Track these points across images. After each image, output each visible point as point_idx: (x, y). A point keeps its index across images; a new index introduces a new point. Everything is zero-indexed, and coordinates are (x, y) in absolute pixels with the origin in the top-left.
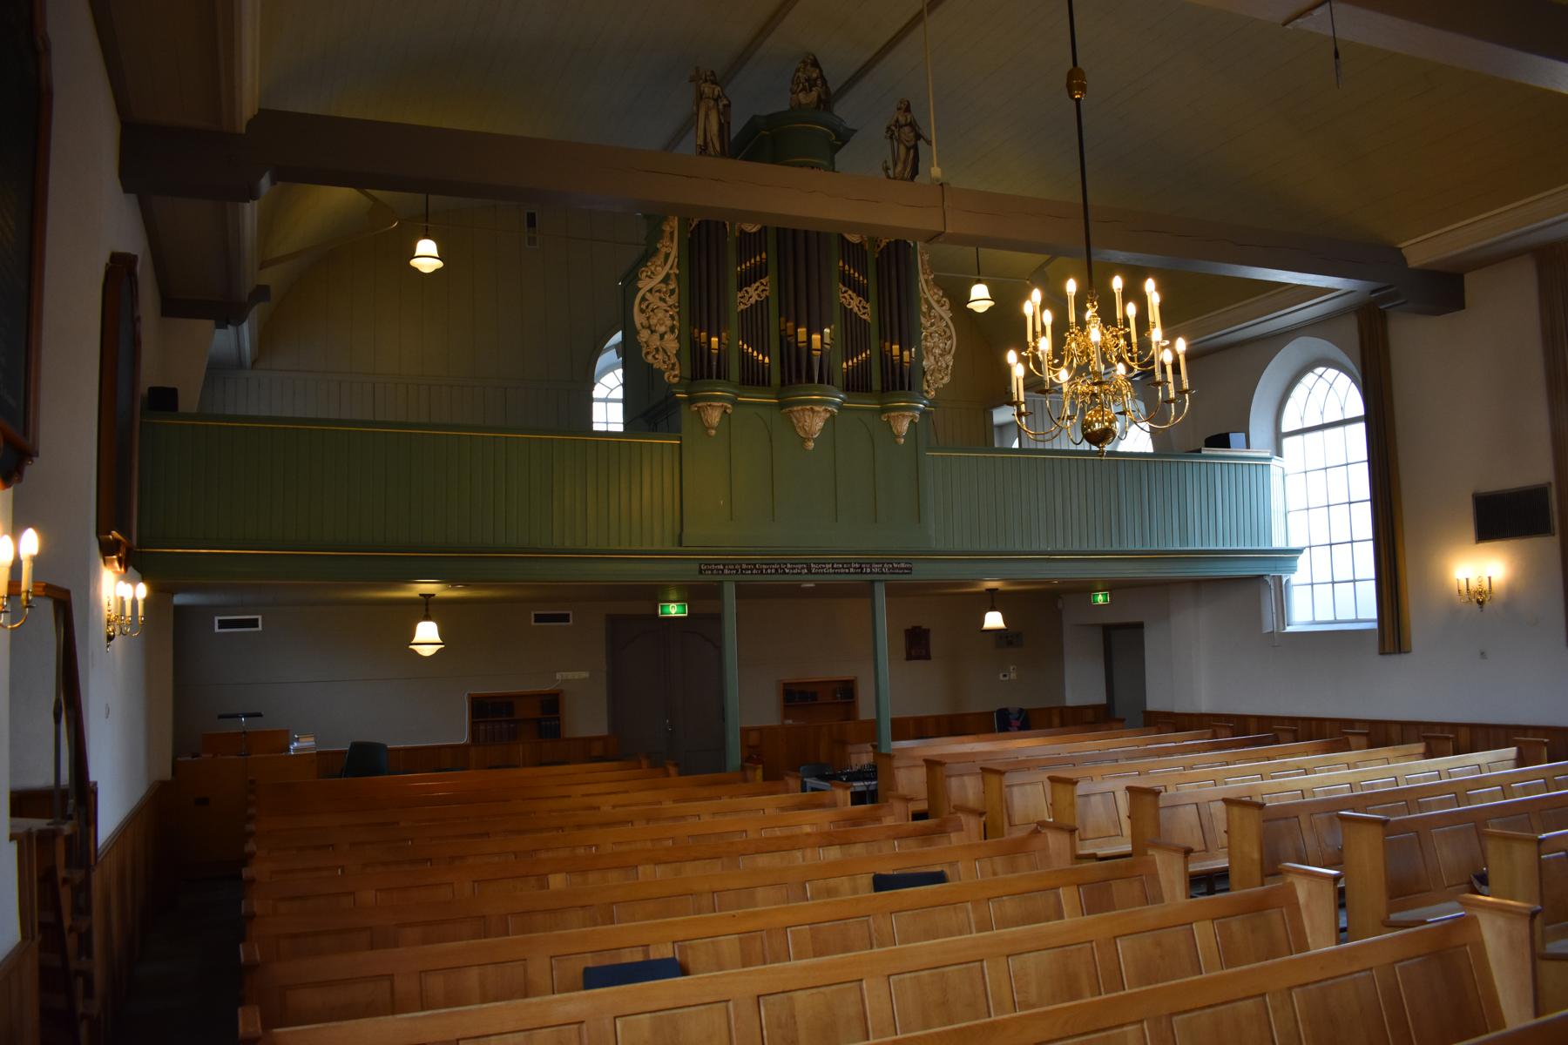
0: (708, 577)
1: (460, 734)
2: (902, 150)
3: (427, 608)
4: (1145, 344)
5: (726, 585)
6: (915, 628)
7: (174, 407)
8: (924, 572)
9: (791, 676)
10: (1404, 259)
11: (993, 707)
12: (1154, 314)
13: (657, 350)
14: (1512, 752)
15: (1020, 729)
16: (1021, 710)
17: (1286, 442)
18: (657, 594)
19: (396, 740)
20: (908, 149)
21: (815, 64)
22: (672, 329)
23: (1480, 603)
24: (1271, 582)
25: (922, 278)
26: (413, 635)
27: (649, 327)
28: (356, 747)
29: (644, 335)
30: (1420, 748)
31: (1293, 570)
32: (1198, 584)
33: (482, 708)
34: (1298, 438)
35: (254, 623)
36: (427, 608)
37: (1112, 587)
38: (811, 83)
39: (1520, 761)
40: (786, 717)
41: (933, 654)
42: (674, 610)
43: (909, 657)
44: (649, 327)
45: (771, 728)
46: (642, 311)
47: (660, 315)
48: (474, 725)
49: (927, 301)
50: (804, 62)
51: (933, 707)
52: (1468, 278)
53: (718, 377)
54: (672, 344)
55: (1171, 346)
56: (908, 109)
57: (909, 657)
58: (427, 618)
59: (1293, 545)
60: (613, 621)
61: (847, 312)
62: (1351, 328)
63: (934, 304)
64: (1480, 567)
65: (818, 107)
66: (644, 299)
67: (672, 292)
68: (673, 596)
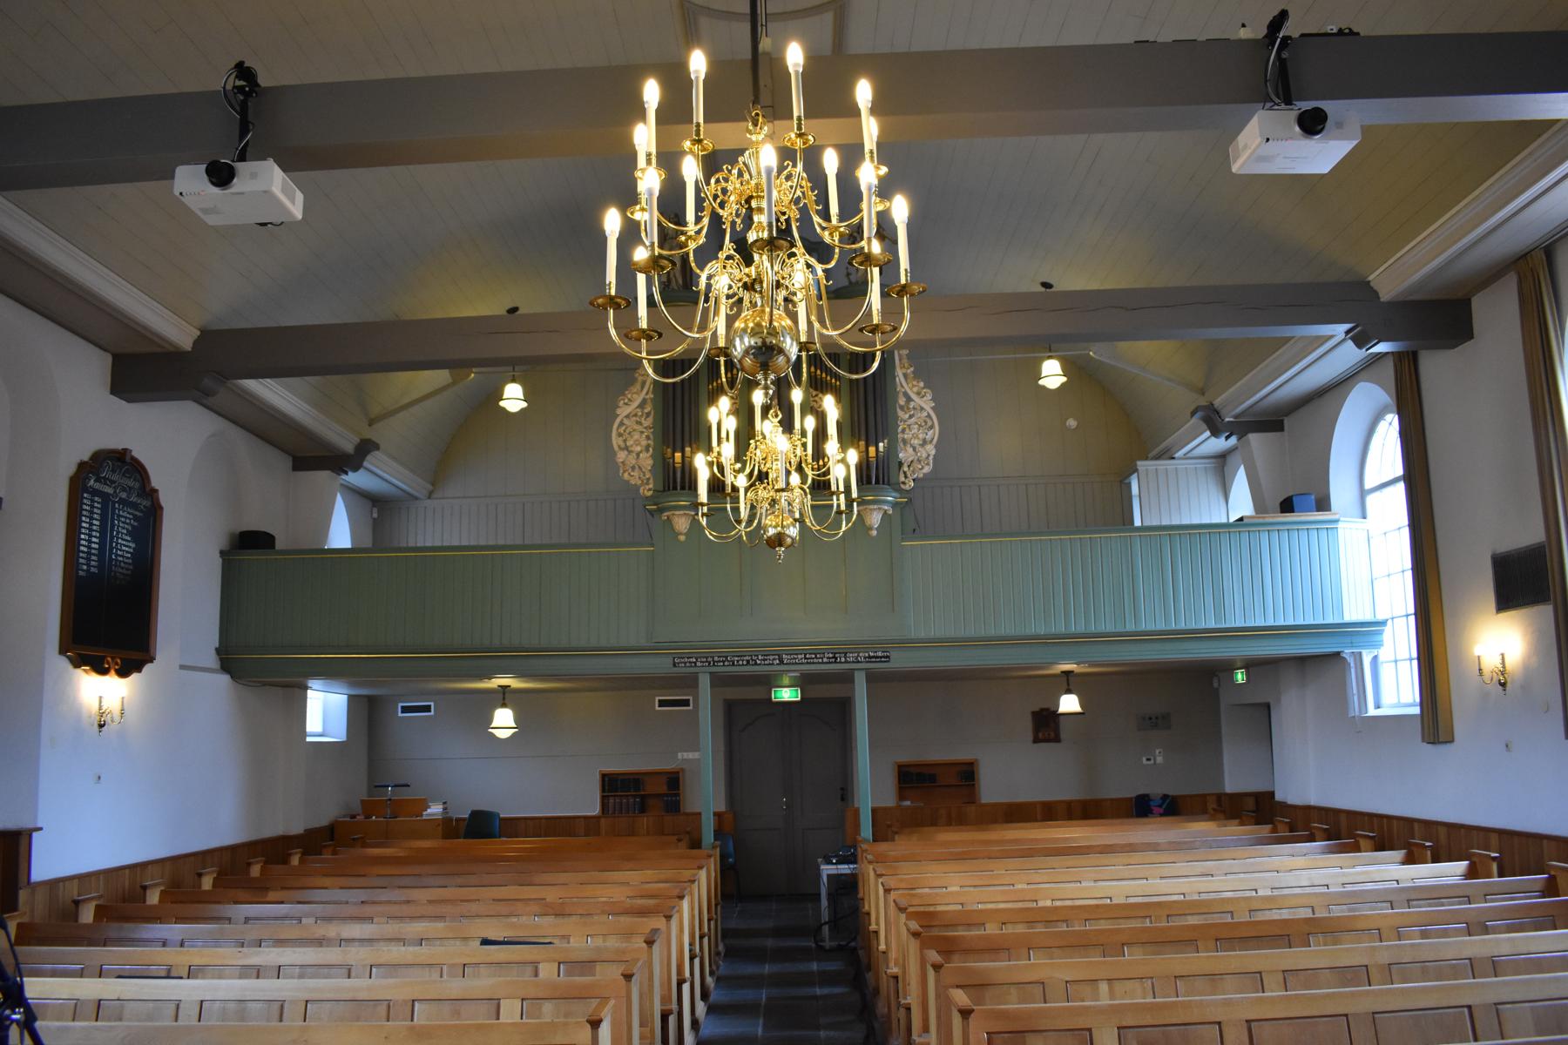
0: (681, 670)
1: (589, 804)
3: (504, 697)
4: (819, 454)
5: (701, 676)
6: (1042, 710)
7: (273, 546)
8: (901, 661)
9: (905, 758)
10: (1376, 293)
11: (1131, 793)
12: (832, 429)
13: (633, 468)
14: (1461, 866)
15: (1161, 815)
16: (1165, 797)
17: (1370, 499)
18: (769, 682)
22: (648, 447)
23: (1503, 685)
24: (1351, 660)
25: (899, 372)
27: (627, 448)
29: (621, 456)
30: (1399, 854)
31: (1378, 645)
32: (1302, 661)
33: (611, 784)
34: (1377, 494)
35: (428, 709)
36: (504, 697)
37: (1250, 665)
39: (1472, 873)
40: (901, 797)
41: (1063, 735)
42: (787, 694)
43: (1036, 740)
44: (627, 448)
45: (885, 809)
46: (620, 435)
47: (636, 436)
49: (906, 394)
52: (1476, 303)
53: (683, 488)
54: (647, 461)
55: (843, 461)
57: (1036, 740)
58: (504, 705)
59: (1380, 617)
62: (1388, 369)
63: (913, 396)
64: (1501, 642)
66: (622, 424)
67: (648, 415)
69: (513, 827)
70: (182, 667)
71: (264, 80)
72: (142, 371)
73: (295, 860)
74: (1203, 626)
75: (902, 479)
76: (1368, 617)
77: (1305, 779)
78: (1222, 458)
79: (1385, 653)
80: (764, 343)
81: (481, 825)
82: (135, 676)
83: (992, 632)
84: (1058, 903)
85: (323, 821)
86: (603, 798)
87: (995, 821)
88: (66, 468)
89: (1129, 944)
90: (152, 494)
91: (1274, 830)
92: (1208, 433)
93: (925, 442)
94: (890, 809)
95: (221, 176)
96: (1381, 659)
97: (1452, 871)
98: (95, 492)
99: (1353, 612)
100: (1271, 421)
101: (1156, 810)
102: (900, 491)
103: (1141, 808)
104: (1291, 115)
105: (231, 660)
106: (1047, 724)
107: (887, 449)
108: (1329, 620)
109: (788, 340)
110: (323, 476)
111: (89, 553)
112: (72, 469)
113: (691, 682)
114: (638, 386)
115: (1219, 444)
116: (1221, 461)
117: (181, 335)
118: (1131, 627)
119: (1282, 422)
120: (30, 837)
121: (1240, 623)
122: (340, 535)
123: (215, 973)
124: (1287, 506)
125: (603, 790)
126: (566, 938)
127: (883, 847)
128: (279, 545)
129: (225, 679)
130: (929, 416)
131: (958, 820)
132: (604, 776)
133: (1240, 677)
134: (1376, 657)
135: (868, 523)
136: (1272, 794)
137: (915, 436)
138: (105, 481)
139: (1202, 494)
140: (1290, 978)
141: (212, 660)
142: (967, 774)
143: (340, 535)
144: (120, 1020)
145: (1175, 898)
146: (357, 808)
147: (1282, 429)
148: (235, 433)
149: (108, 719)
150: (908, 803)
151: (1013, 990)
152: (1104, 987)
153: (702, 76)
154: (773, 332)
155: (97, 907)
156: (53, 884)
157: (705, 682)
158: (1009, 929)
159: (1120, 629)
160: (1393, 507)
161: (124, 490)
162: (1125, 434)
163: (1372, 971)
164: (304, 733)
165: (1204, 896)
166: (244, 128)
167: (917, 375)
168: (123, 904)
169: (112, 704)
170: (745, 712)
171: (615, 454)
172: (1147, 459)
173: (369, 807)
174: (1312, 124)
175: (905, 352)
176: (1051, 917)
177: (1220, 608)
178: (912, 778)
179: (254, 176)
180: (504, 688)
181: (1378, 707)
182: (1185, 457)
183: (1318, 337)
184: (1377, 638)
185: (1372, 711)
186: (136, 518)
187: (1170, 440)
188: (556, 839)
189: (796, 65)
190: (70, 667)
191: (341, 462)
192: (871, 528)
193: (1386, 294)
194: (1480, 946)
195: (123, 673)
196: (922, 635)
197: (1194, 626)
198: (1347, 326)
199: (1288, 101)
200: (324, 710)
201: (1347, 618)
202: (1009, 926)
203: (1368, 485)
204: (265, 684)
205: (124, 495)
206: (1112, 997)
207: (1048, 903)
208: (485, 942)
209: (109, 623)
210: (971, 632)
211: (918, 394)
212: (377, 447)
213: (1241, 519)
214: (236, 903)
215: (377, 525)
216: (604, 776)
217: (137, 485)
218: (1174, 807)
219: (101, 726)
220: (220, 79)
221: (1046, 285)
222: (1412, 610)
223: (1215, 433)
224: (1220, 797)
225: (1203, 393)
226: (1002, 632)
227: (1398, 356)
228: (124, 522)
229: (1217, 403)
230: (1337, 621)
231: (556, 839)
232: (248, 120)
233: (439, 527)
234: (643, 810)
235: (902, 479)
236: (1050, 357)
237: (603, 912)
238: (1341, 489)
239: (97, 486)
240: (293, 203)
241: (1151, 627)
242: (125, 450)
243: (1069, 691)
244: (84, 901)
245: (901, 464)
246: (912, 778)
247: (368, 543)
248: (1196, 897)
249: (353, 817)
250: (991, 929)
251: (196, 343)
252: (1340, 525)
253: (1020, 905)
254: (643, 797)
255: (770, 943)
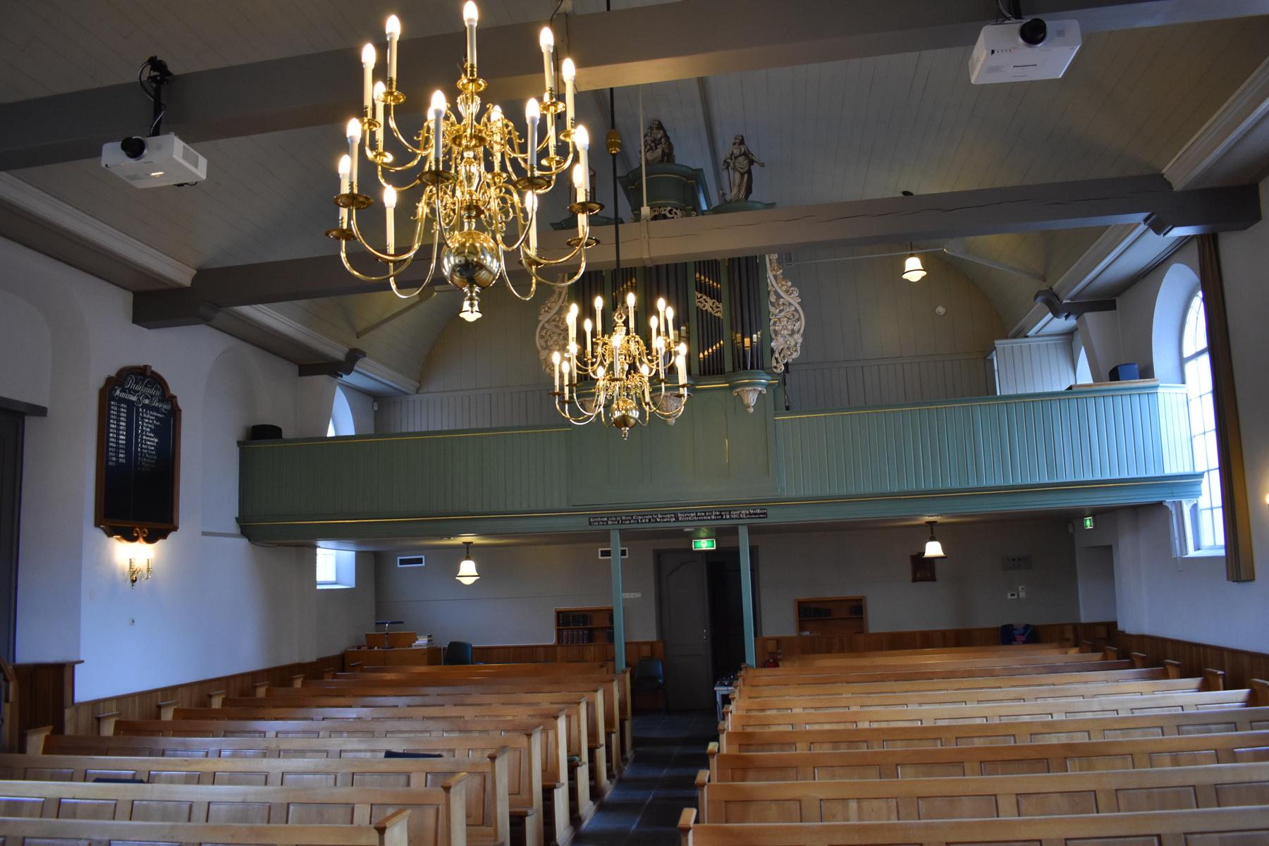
0: (596, 527)
2: (737, 176)
3: (468, 551)
8: (776, 517)
10: (1169, 185)
11: (999, 623)
14: (1243, 693)
15: (1025, 642)
16: (1027, 627)
17: (1189, 367)
19: (478, 641)
20: (742, 175)
21: (660, 126)
25: (770, 274)
26: (458, 571)
28: (453, 645)
30: (1195, 682)
32: (1136, 510)
33: (565, 619)
35: (420, 561)
37: (1097, 513)
38: (656, 142)
39: (1252, 701)
40: (801, 628)
42: (704, 545)
43: (915, 580)
46: (542, 337)
47: (555, 338)
48: (559, 632)
49: (776, 293)
50: (651, 128)
51: (941, 621)
56: (742, 142)
57: (915, 580)
58: (468, 558)
59: (1198, 470)
60: (659, 556)
61: (702, 313)
62: (1193, 251)
63: (782, 294)
65: (662, 161)
66: (543, 328)
68: (703, 535)
69: (486, 655)
70: (204, 534)
71: (175, 68)
72: (156, 304)
73: (298, 684)
74: (1037, 481)
75: (774, 364)
76: (1188, 470)
77: (1141, 614)
78: (1070, 334)
79: (1203, 502)
80: (467, 261)
81: (457, 654)
82: (160, 542)
83: (853, 491)
84: (875, 725)
85: (335, 650)
86: (558, 631)
87: (880, 649)
88: (96, 381)
89: (902, 765)
90: (172, 400)
91: (1105, 658)
92: (1050, 315)
93: (793, 333)
94: (792, 638)
95: (134, 149)
96: (1201, 506)
97: (1234, 698)
98: (121, 400)
99: (1174, 465)
100: (1106, 300)
101: (1018, 637)
102: (771, 374)
103: (1006, 636)
104: (1015, 26)
105: (249, 527)
106: (923, 568)
107: (761, 340)
108: (1152, 474)
109: (489, 258)
110: (322, 379)
111: (117, 448)
112: (101, 383)
113: (605, 537)
114: (556, 296)
115: (1062, 323)
116: (1069, 336)
117: (182, 275)
118: (973, 484)
119: (1114, 301)
120: (73, 668)
121: (1070, 479)
122: (342, 422)
123: (219, 775)
124: (1114, 375)
125: (558, 624)
126: (452, 751)
127: (766, 674)
128: (285, 435)
129: (244, 542)
130: (796, 310)
131: (850, 648)
132: (559, 613)
133: (1088, 523)
134: (1195, 506)
135: (746, 402)
136: (1115, 623)
137: (785, 328)
138: (131, 391)
139: (1045, 365)
140: (1024, 803)
141: (233, 527)
142: (857, 608)
143: (342, 422)
144: (75, 817)
145: (978, 721)
146: (364, 640)
147: (1114, 308)
148: (245, 348)
149: (138, 576)
150: (807, 633)
151: (774, 807)
152: (853, 805)
153: (396, 38)
154: (473, 250)
155: (117, 722)
156: (95, 704)
157: (615, 537)
158: (817, 750)
159: (964, 486)
160: (1201, 373)
161: (146, 397)
162: (982, 319)
163: (1101, 797)
164: (315, 583)
165: (1005, 720)
166: (158, 108)
167: (786, 277)
168: (144, 722)
169: (141, 564)
170: (666, 556)
171: (538, 352)
172: (1006, 338)
173: (372, 640)
174: (1034, 34)
175: (774, 257)
176: (854, 738)
177: (1052, 465)
178: (809, 612)
179: (159, 147)
180: (468, 544)
181: (1197, 548)
182: (1037, 335)
183: (1129, 225)
184: (1197, 488)
185: (1192, 553)
186: (158, 419)
187: (1021, 323)
188: (518, 662)
189: (470, 20)
190: (105, 536)
191: (335, 368)
192: (749, 407)
193: (1178, 186)
194: (1227, 771)
195: (150, 539)
196: (793, 494)
197: (1029, 482)
198: (1145, 215)
199: (1018, 16)
200: (333, 564)
201: (1167, 472)
202: (817, 746)
203: (1186, 354)
204: (279, 545)
205: (147, 402)
206: (860, 819)
207: (866, 725)
208: (389, 754)
209: (138, 498)
210: (836, 491)
211: (787, 291)
212: (364, 354)
213: (1070, 388)
214: (319, 707)
215: (378, 417)
216: (559, 613)
217: (158, 393)
218: (1034, 636)
219: (134, 581)
220: (134, 72)
221: (906, 193)
222: (1216, 465)
223: (1056, 314)
224: (1076, 627)
225: (1044, 279)
226: (801, 494)
227: (1200, 238)
228: (148, 421)
229: (1055, 287)
230: (1158, 474)
231: (518, 662)
232: (162, 100)
233: (425, 416)
234: (591, 639)
235: (774, 364)
236: (912, 255)
237: (496, 729)
238: (1162, 360)
239: (123, 395)
240: (196, 167)
241: (992, 483)
242: (146, 367)
243: (933, 539)
244: (104, 718)
245: (773, 351)
246: (809, 612)
247: (371, 431)
248: (997, 721)
249: (359, 647)
250: (801, 749)
251: (194, 280)
252: (1160, 390)
253: (842, 727)
254: (590, 630)
255: (676, 750)
